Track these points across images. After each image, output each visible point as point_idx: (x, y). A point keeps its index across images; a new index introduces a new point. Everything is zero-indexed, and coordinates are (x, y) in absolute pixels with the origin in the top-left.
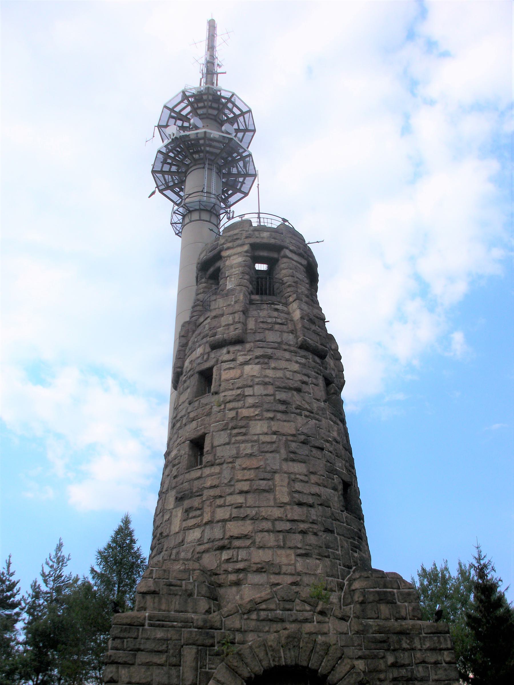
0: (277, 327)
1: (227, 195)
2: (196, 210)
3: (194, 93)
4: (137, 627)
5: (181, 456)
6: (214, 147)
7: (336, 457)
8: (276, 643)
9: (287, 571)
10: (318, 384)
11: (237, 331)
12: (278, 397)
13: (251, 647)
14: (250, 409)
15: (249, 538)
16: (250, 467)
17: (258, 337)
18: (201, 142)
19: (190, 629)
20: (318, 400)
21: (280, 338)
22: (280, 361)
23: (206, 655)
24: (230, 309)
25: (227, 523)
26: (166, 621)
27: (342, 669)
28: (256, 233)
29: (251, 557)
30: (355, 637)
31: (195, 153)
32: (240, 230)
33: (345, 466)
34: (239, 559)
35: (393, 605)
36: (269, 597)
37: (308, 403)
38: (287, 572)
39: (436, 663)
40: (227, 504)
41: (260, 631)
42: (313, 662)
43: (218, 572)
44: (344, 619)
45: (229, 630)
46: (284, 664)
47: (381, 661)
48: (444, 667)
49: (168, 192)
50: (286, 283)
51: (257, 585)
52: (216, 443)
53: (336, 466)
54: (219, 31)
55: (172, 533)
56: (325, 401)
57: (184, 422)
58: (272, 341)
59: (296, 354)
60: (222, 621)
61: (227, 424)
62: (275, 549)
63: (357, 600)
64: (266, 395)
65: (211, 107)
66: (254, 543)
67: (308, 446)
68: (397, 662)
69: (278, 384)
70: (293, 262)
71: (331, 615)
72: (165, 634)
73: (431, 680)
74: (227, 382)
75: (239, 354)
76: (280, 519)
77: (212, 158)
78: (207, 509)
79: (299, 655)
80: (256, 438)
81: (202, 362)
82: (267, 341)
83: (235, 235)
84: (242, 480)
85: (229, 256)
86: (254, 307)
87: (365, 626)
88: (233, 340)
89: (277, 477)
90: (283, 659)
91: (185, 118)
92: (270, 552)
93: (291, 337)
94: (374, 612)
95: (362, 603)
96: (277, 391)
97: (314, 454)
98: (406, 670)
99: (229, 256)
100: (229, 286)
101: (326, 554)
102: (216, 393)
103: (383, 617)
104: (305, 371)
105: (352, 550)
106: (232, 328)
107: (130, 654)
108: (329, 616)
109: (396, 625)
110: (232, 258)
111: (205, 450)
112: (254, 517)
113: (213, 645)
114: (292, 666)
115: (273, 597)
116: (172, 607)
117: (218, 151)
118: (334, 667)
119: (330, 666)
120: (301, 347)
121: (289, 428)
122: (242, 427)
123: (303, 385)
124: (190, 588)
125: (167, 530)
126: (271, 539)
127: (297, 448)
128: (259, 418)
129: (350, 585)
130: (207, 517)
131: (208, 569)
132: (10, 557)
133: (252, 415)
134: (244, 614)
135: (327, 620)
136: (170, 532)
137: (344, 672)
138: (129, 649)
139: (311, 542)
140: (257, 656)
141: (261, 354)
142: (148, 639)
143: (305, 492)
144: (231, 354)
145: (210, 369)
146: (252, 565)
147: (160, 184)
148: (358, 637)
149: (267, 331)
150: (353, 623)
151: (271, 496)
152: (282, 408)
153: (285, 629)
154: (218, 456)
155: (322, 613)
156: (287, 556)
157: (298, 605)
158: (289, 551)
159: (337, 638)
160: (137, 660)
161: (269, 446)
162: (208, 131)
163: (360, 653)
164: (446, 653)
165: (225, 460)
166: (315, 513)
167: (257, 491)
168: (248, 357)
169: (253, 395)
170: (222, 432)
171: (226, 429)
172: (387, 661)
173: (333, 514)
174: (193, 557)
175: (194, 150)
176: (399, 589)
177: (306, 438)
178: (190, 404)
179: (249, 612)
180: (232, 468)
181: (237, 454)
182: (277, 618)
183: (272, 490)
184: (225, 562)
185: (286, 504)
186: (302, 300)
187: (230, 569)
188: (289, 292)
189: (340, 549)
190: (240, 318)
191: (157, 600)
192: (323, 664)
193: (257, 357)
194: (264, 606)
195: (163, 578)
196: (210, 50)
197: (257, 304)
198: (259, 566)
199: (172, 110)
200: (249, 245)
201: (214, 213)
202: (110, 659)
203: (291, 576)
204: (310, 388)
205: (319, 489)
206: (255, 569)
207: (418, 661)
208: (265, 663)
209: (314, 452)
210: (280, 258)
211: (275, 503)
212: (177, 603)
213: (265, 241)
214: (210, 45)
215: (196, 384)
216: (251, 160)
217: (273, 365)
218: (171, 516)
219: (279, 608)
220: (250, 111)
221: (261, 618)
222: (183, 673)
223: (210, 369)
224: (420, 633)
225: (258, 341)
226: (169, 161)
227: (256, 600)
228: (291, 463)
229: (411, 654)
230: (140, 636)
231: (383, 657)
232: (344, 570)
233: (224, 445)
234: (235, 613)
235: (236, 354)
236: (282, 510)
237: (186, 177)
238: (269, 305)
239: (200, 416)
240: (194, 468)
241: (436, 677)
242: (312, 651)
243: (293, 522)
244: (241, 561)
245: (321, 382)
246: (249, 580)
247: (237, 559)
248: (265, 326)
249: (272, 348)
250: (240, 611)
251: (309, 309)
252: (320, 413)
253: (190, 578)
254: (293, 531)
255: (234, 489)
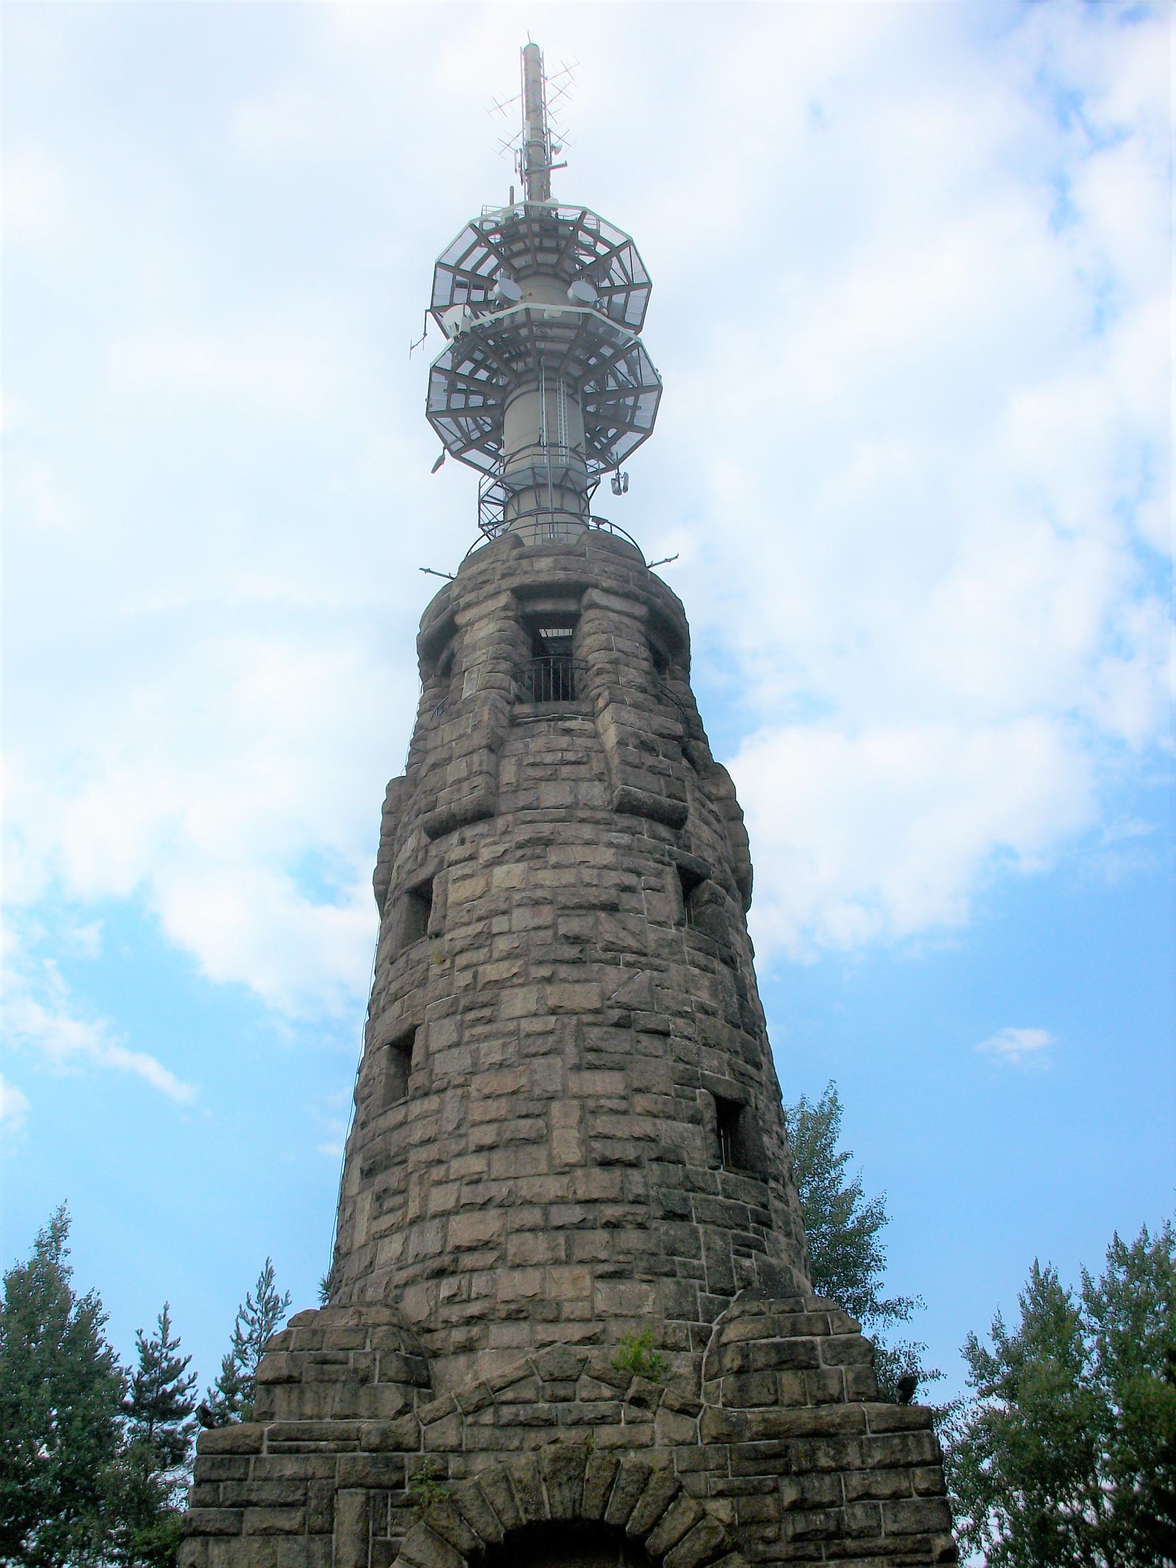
0: (565, 770)
1: (605, 441)
2: (528, 488)
3: (497, 224)
4: (247, 1456)
5: (374, 1079)
6: (552, 339)
7: (704, 1048)
8: (530, 1474)
9: (572, 1313)
10: (663, 887)
11: (476, 793)
12: (562, 930)
13: (477, 1485)
14: (501, 963)
15: (492, 1249)
16: (497, 1093)
17: (523, 799)
18: (524, 332)
19: (354, 1454)
20: (660, 924)
21: (573, 796)
22: (569, 848)
23: (386, 1505)
24: (465, 746)
25: (452, 1218)
26: (304, 1440)
27: (677, 1521)
28: (524, 562)
29: (496, 1290)
30: (711, 1450)
31: (512, 359)
32: (490, 561)
33: (729, 1065)
34: (473, 1295)
35: (812, 1372)
36: (521, 1373)
37: (633, 934)
38: (572, 1317)
39: (896, 1496)
40: (452, 1177)
41: (501, 1450)
42: (613, 1509)
43: (432, 1326)
44: (686, 1411)
45: (433, 1451)
46: (549, 1517)
47: (769, 1500)
48: (913, 1502)
49: (473, 455)
50: (594, 666)
51: (508, 1348)
52: (434, 1047)
53: (702, 1068)
54: (549, 68)
55: (356, 1245)
56: (679, 924)
57: (382, 1003)
58: (552, 804)
59: (609, 826)
60: (419, 1432)
61: (457, 999)
62: (548, 1267)
63: (729, 1366)
64: (536, 928)
65: (541, 249)
66: (502, 1258)
67: (632, 1032)
68: (804, 1500)
69: (562, 899)
70: (611, 614)
71: (658, 1406)
72: (301, 1468)
73: (883, 1534)
74: (459, 908)
75: (483, 842)
76: (561, 1201)
77: (556, 364)
78: (414, 1191)
79: (582, 1495)
80: (512, 1026)
81: (414, 867)
82: (542, 805)
83: (480, 573)
84: (482, 1123)
85: (470, 624)
86: (520, 731)
87: (734, 1425)
88: (469, 815)
89: (556, 1108)
90: (547, 1506)
91: (487, 283)
92: (535, 1275)
93: (597, 789)
94: (765, 1391)
95: (741, 1371)
96: (560, 916)
97: (646, 1047)
98: (827, 1515)
99: (470, 624)
100: (466, 694)
101: (666, 1269)
102: (438, 935)
103: (786, 1399)
104: (628, 862)
105: (737, 1252)
106: (466, 786)
107: (232, 1512)
108: (654, 1407)
109: (806, 1416)
110: (476, 626)
111: (414, 1062)
112: (505, 1201)
113: (400, 1485)
114: (566, 1521)
115: (532, 1374)
116: (327, 1409)
117: (564, 347)
118: (660, 1517)
119: (651, 1516)
120: (621, 809)
121: (584, 996)
122: (484, 1006)
123: (624, 895)
124: (363, 1366)
125: (348, 1241)
126: (538, 1247)
127: (602, 1039)
128: (521, 981)
129: (720, 1333)
130: (413, 1210)
131: (414, 1321)
132: (166, 1309)
133: (505, 975)
134: (467, 1414)
135: (649, 1415)
136: (352, 1246)
137: (681, 1528)
138: (228, 1503)
139: (630, 1245)
140: (492, 1503)
141: (527, 837)
142: (266, 1479)
143: (619, 1134)
144: (468, 845)
145: (428, 883)
146: (498, 1307)
147: (450, 438)
148: (718, 1450)
149: (543, 784)
150: (706, 1422)
151: (541, 1152)
152: (572, 952)
153: (555, 1441)
154: (437, 1075)
155: (638, 1402)
156: (575, 1280)
157: (585, 1388)
158: (578, 1270)
159: (671, 1453)
160: (244, 1525)
161: (540, 1041)
162: (532, 306)
163: (721, 1485)
164: (918, 1472)
165: (449, 1082)
166: (642, 1180)
167: (513, 1143)
168: (501, 849)
169: (510, 932)
170: (446, 1021)
171: (454, 1013)
172: (782, 1500)
173: (687, 1177)
174: (387, 1296)
175: (510, 352)
176: (829, 1334)
177: (625, 1013)
178: (392, 963)
179: (478, 1408)
180: (463, 1097)
181: (474, 1064)
182: (537, 1418)
183: (544, 1139)
184: (445, 1302)
185: (573, 1166)
186: (623, 702)
187: (454, 1319)
188: (598, 687)
189: (703, 1253)
190: (481, 762)
191: (295, 1395)
192: (635, 1513)
193: (520, 846)
194: (509, 1395)
195: (310, 1347)
196: (533, 116)
197: (527, 723)
198: (513, 1307)
199: (456, 269)
200: (509, 592)
201: (568, 489)
202: (190, 1525)
203: (581, 1324)
204: (640, 900)
205: (655, 1125)
206: (503, 1314)
207: (854, 1495)
208: (508, 1518)
209: (644, 1044)
210: (582, 612)
211: (550, 1165)
212: (337, 1399)
213: (544, 578)
214: (531, 105)
215: (404, 918)
216: (642, 354)
217: (553, 859)
218: (354, 1211)
219: (543, 1397)
220: (629, 243)
221: (503, 1421)
222: (337, 1545)
223: (428, 883)
224: (862, 1432)
225: (523, 808)
226: (461, 386)
227: (493, 1383)
228: (587, 1075)
229: (840, 1481)
230: (251, 1475)
231: (776, 1490)
232: (711, 1301)
233: (450, 1047)
234: (448, 1413)
235: (478, 844)
236: (565, 1179)
237: (503, 414)
238: (552, 723)
239: (407, 988)
240: (394, 1105)
241: (894, 1528)
242: (610, 1486)
243: (590, 1205)
244: (477, 1298)
245: (671, 881)
246: (492, 1337)
247: (469, 1296)
248: (538, 773)
249: (552, 821)
250: (460, 1410)
251: (640, 718)
252: (665, 952)
253: (365, 1343)
254: (589, 1224)
255: (467, 1144)
